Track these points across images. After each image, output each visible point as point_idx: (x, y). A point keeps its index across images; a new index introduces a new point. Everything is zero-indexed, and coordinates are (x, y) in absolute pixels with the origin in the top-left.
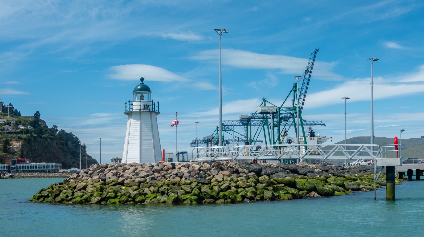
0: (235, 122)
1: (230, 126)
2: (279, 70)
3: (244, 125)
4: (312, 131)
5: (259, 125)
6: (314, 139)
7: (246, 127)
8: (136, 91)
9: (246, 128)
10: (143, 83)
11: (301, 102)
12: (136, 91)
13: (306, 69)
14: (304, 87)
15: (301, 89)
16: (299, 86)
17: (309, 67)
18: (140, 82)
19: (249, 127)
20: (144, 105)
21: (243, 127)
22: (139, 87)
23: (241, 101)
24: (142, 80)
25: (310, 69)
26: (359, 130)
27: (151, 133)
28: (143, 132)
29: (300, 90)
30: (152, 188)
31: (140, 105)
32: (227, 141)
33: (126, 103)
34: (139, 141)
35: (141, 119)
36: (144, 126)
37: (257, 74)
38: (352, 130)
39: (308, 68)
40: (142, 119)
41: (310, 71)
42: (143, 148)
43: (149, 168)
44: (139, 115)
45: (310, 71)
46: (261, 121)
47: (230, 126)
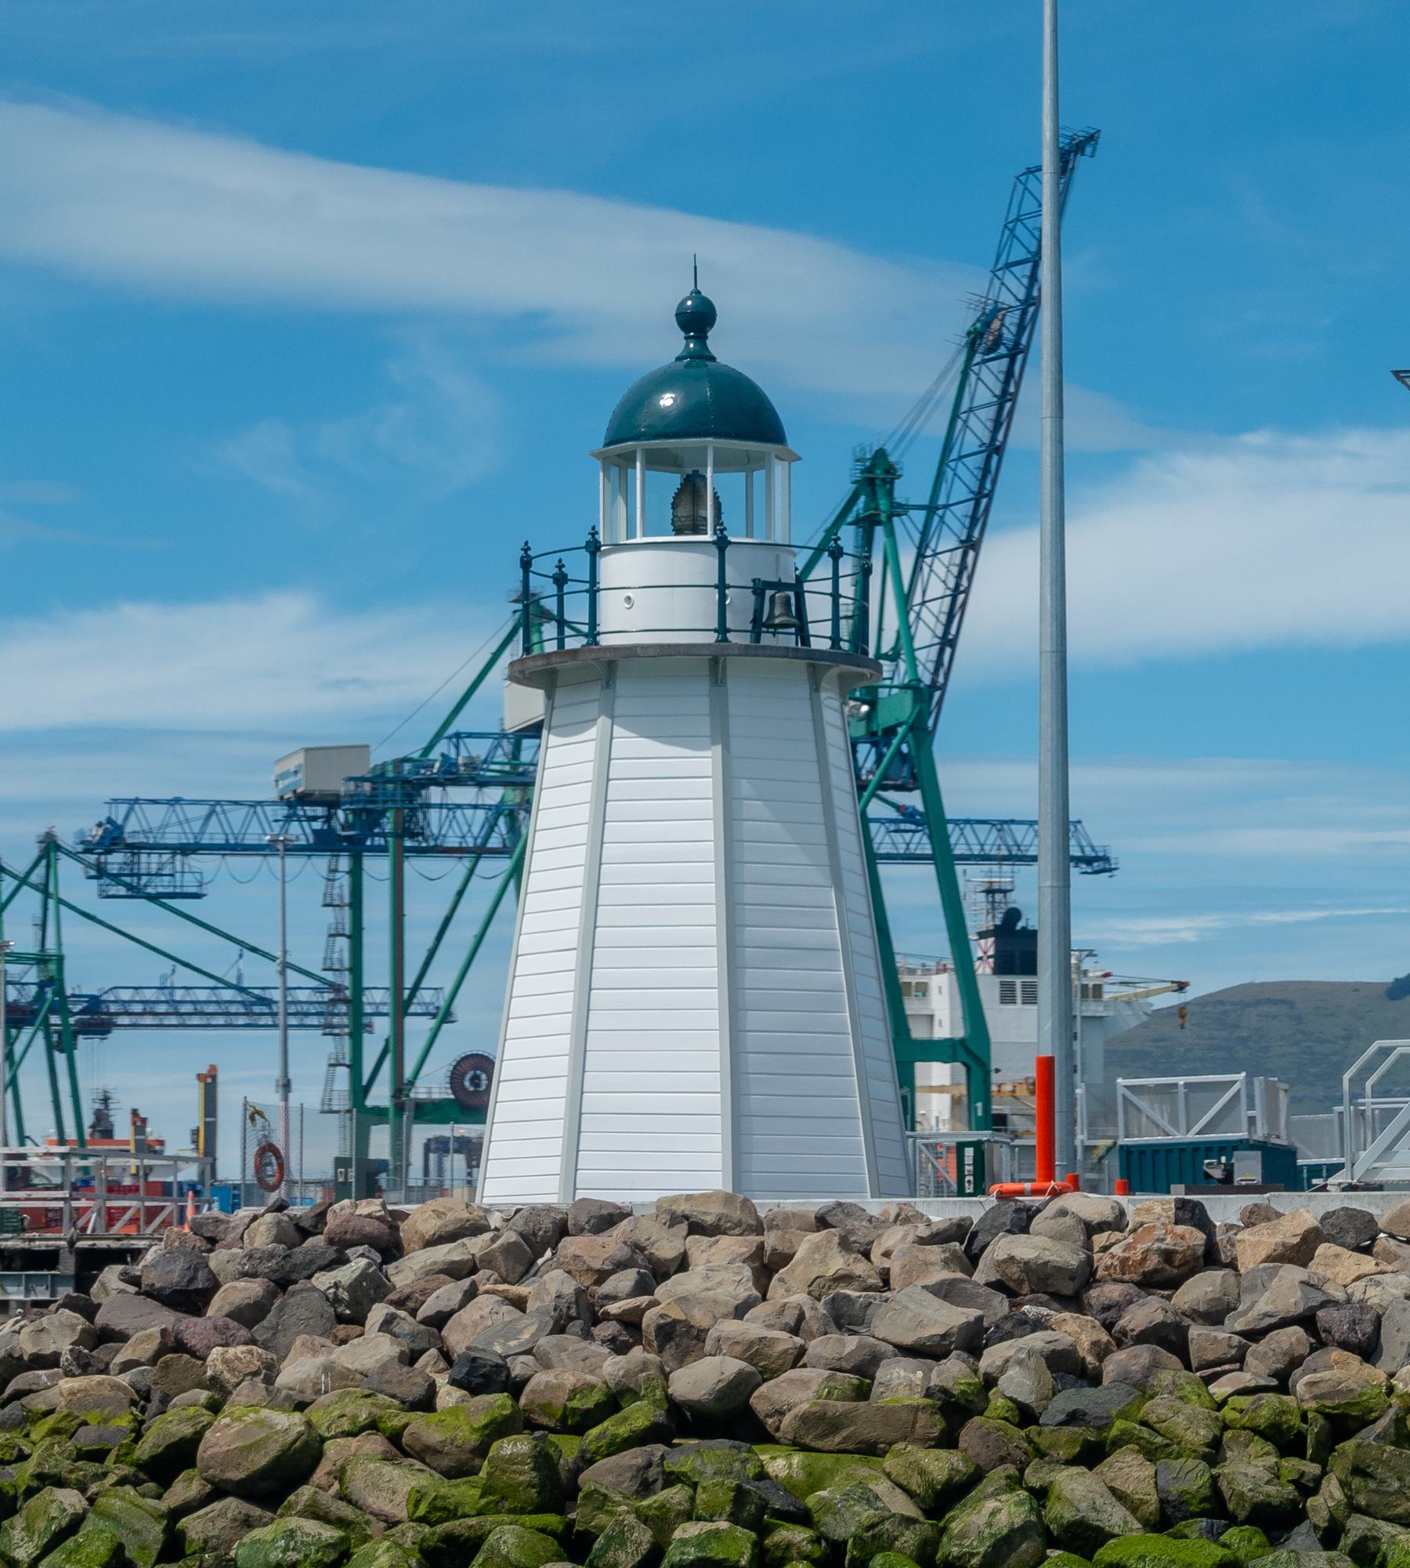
0: (237, 816)
1: (185, 850)
2: (533, 325)
3: (325, 842)
4: (1013, 915)
5: (480, 852)
6: (1031, 997)
7: (344, 863)
8: (632, 436)
9: (344, 881)
10: (702, 356)
11: (925, 636)
12: (632, 436)
13: (968, 319)
14: (960, 492)
15: (931, 509)
16: (912, 488)
17: (1007, 299)
18: (676, 343)
19: (377, 867)
20: (759, 588)
21: (321, 862)
22: (667, 400)
23: (137, 615)
24: (697, 319)
25: (1012, 319)
26: (1272, 917)
27: (821, 876)
28: (749, 871)
29: (919, 516)
30: (1129, 1470)
31: (722, 586)
32: (94, 1004)
33: (526, 564)
34: (709, 966)
35: (721, 734)
36: (752, 807)
37: (310, 355)
38: (1209, 921)
39: (991, 315)
40: (735, 727)
41: (1008, 335)
42: (752, 1040)
43: (936, 1253)
44: (704, 686)
45: (1008, 335)
46: (497, 810)
47: (185, 850)
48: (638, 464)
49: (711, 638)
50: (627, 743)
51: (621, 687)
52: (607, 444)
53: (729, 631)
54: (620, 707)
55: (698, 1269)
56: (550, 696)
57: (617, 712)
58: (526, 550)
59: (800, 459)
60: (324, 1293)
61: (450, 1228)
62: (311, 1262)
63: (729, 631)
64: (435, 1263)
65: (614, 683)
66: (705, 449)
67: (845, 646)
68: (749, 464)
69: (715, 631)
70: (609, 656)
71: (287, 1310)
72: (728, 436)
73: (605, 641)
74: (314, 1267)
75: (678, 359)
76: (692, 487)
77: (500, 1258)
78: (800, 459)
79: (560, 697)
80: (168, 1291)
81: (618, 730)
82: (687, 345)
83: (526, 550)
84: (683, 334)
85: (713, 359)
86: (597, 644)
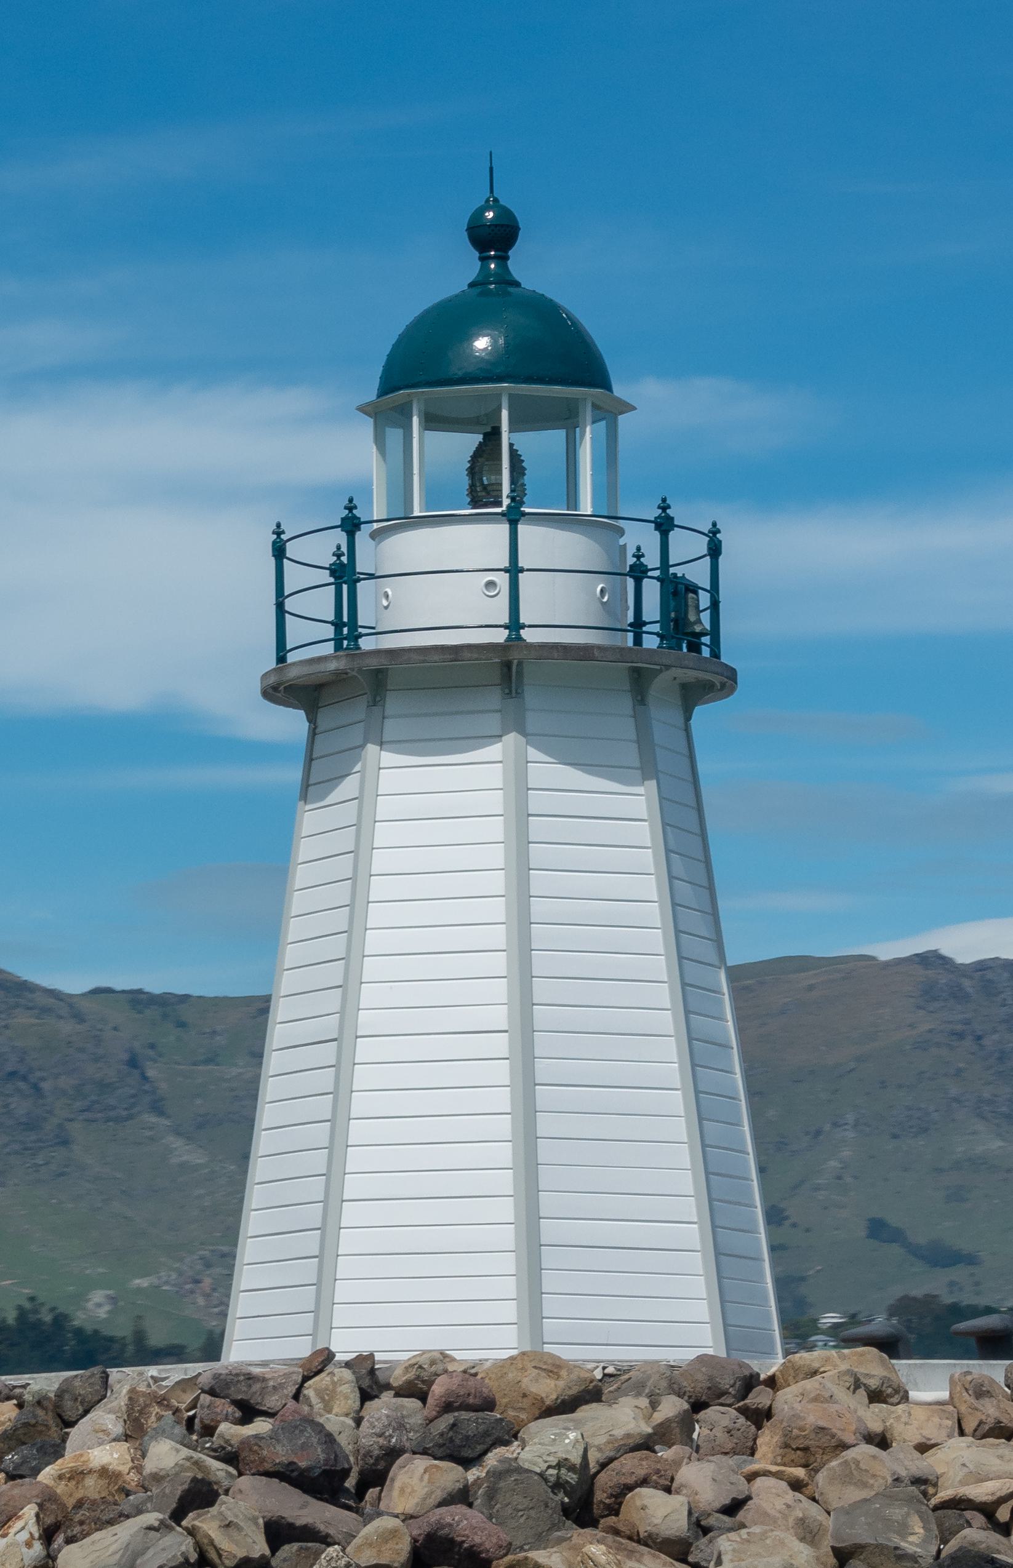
48: (415, 420)
49: (500, 636)
50: (544, 770)
51: (531, 697)
52: (379, 396)
53: (523, 627)
54: (533, 721)
55: (225, 1506)
56: (312, 719)
57: (530, 728)
58: (278, 533)
59: (634, 408)
60: (541, 1475)
61: (575, 1390)
62: (486, 1434)
63: (523, 627)
64: (628, 1436)
65: (384, 699)
66: (498, 397)
67: (651, 642)
68: (566, 418)
69: (506, 627)
70: (374, 663)
71: (500, 1497)
72: (529, 380)
73: (367, 644)
74: (489, 1441)
75: (471, 285)
76: (487, 451)
77: (677, 1430)
78: (634, 408)
79: (325, 719)
80: (317, 1472)
81: (533, 753)
82: (484, 268)
83: (278, 533)
84: (477, 254)
85: (517, 284)
86: (359, 648)
